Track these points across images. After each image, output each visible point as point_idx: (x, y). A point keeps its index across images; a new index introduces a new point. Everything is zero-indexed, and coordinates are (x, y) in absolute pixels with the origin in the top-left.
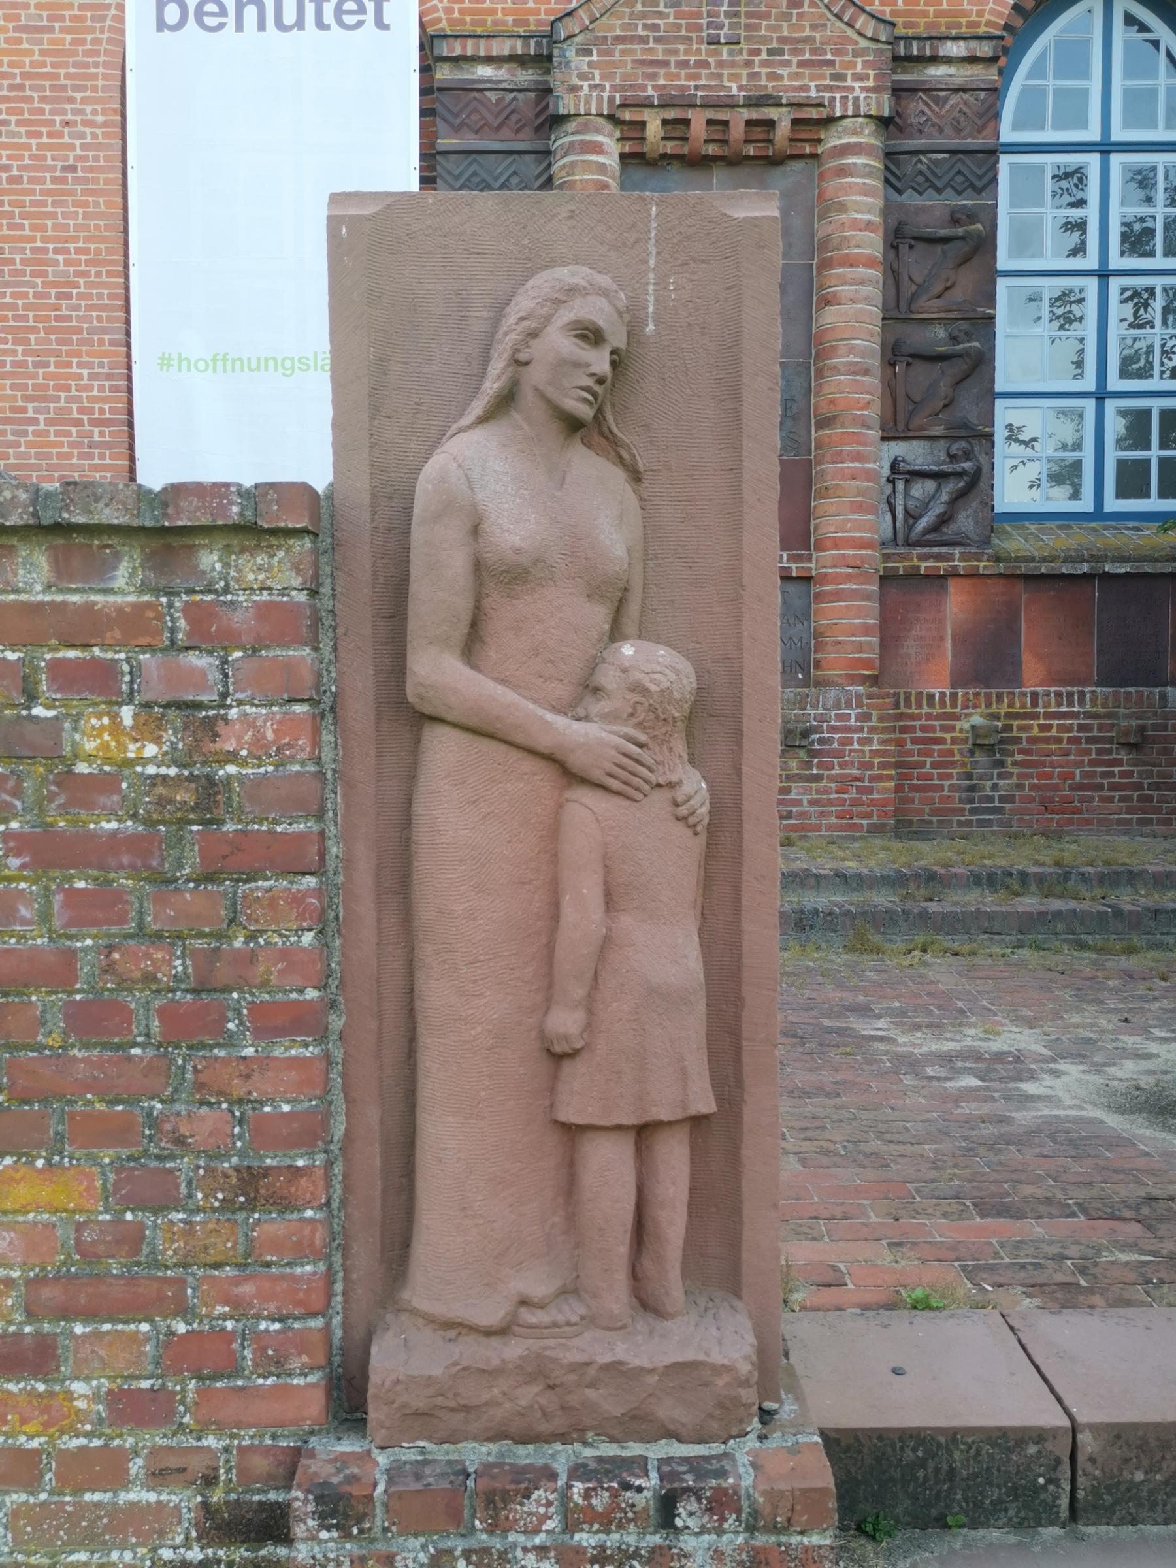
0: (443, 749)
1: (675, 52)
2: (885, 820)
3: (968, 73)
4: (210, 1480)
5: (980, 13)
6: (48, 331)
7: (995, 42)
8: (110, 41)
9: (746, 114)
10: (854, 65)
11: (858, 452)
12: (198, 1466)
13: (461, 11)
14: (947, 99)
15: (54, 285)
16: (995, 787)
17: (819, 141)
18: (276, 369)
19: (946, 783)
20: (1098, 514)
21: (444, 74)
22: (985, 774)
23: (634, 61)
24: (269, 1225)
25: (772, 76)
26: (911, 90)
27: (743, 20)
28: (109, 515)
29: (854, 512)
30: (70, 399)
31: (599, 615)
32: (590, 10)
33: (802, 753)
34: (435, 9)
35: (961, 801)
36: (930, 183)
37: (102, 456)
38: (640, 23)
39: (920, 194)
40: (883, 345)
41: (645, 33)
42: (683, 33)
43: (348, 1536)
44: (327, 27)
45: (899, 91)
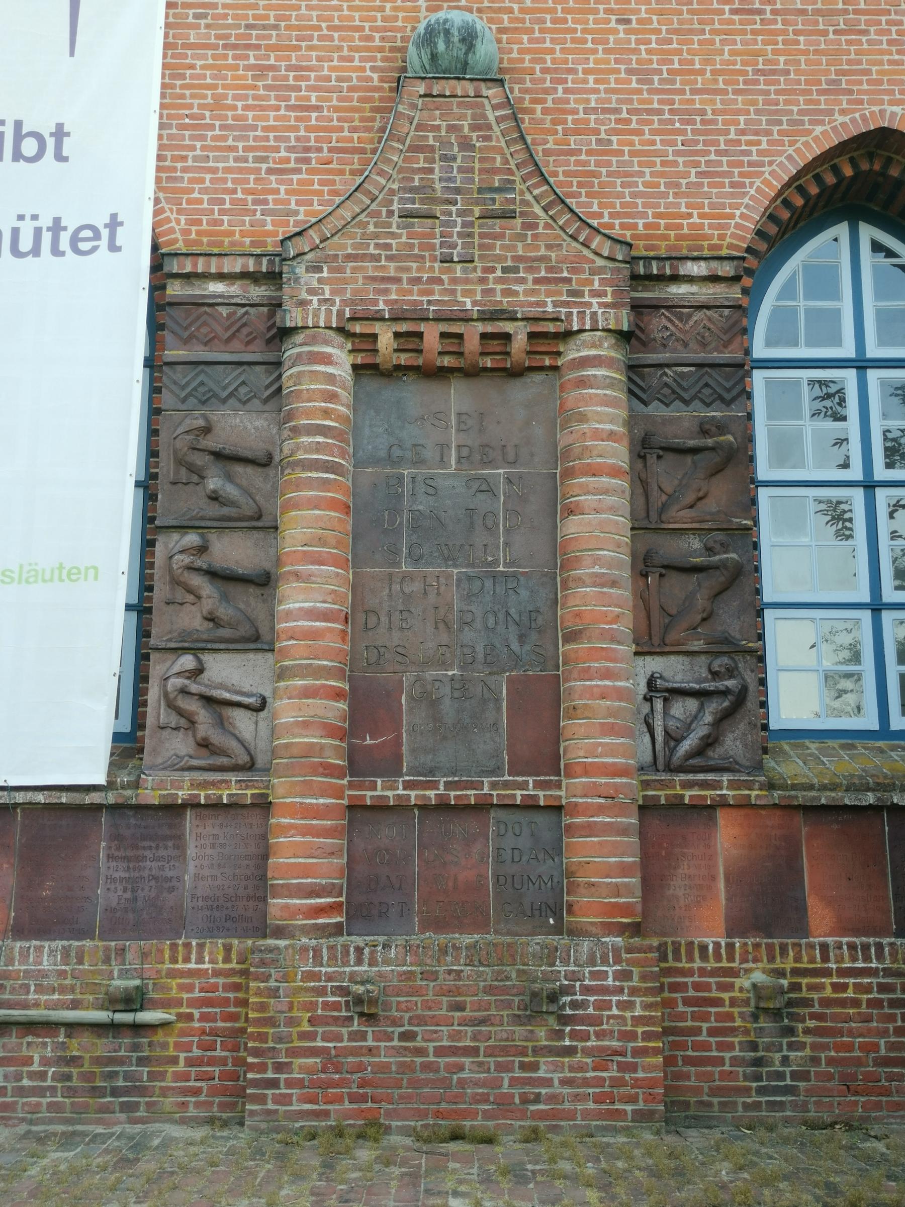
1: (408, 270)
2: (652, 1106)
3: (711, 291)
5: (722, 237)
7: (735, 262)
9: (481, 327)
10: (591, 282)
11: (608, 669)
13: (198, 233)
14: (690, 316)
16: (785, 1060)
17: (559, 354)
18: (44, 570)
19: (727, 1055)
20: (884, 731)
21: (175, 289)
22: (773, 1044)
23: (365, 278)
25: (507, 292)
26: (655, 307)
27: (476, 240)
29: (604, 734)
32: (320, 230)
33: (552, 1021)
34: (172, 231)
35: (746, 1078)
36: (675, 395)
38: (372, 242)
39: (667, 405)
40: (634, 555)
41: (377, 252)
42: (416, 251)
44: (63, 254)
45: (637, 308)
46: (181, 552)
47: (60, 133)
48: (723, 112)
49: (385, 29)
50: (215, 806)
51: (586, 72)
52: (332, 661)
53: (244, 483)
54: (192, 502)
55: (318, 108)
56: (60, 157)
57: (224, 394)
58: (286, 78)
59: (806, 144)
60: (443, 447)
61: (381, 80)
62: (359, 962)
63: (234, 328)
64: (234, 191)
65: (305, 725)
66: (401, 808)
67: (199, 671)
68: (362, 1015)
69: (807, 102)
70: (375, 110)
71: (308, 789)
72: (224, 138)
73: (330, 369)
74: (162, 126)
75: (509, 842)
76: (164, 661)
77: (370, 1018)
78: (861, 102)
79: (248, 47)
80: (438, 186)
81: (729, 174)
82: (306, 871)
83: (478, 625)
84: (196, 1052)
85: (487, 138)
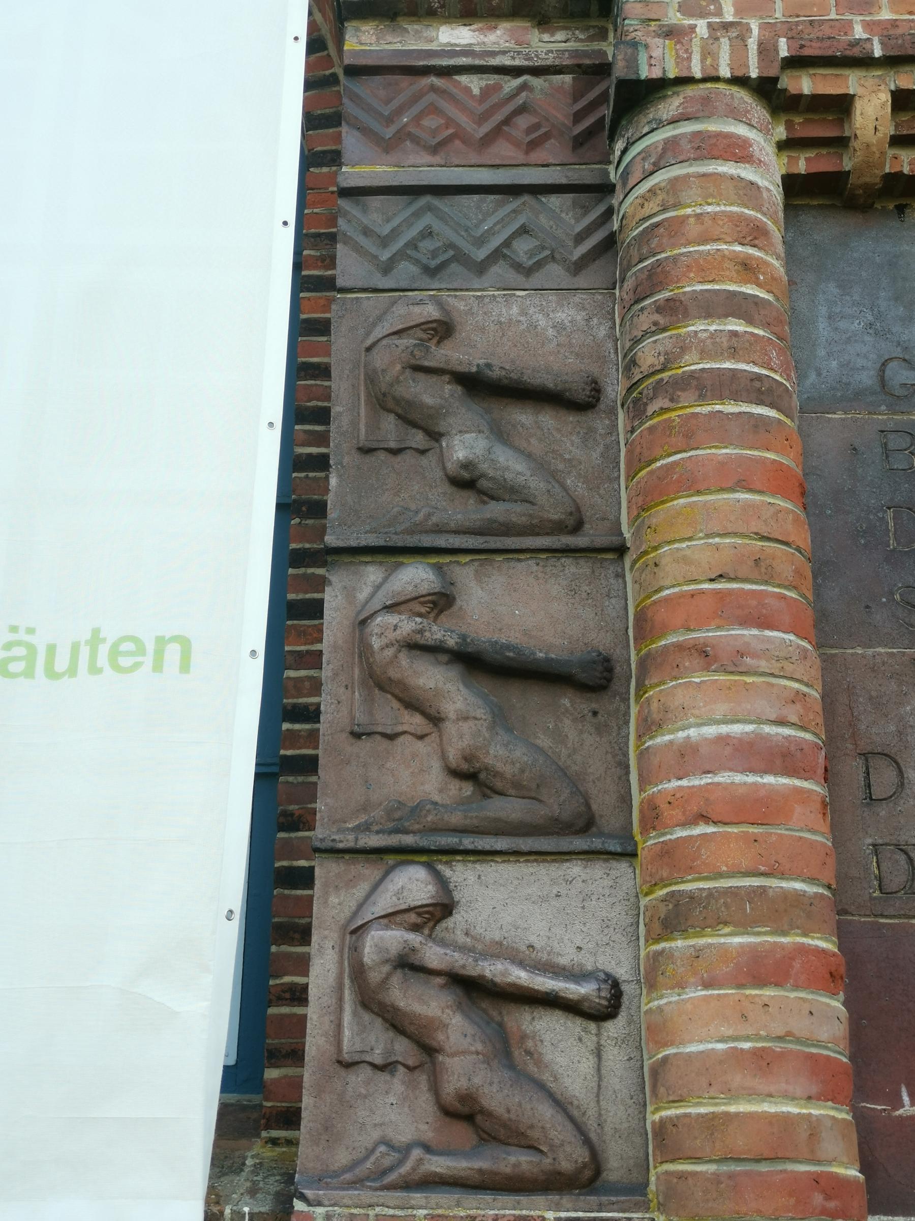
18: (51, 649)
44: (100, 671)
46: (389, 608)
52: (812, 880)
53: (536, 446)
54: (414, 495)
57: (481, 254)
63: (499, 117)
65: (763, 1061)
67: (442, 909)
73: (747, 173)
76: (351, 883)
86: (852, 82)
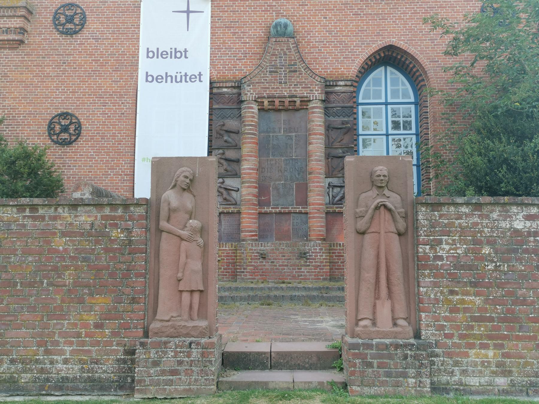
0: (164, 235)
1: (271, 85)
4: (125, 345)
5: (349, 74)
6: (115, 152)
8: (134, 84)
9: (289, 99)
12: (123, 343)
14: (340, 95)
15: (117, 141)
21: (215, 91)
24: (136, 306)
25: (295, 91)
26: (332, 93)
28: (118, 202)
29: (317, 196)
30: (119, 169)
31: (187, 216)
34: (214, 75)
36: (336, 115)
37: (126, 183)
40: (325, 154)
43: (144, 349)
45: (327, 93)
47: (186, 51)
48: (350, 41)
49: (265, 22)
50: (228, 213)
51: (316, 32)
54: (221, 143)
55: (249, 43)
56: (186, 57)
58: (241, 35)
59: (371, 49)
60: (280, 128)
61: (264, 35)
62: (262, 246)
64: (228, 65)
65: (249, 194)
66: (271, 213)
68: (262, 257)
69: (371, 38)
70: (263, 43)
71: (249, 209)
72: (226, 51)
73: (253, 110)
74: (211, 49)
75: (295, 221)
77: (264, 258)
78: (385, 38)
79: (231, 27)
80: (278, 64)
81: (351, 58)
82: (249, 227)
83: (288, 171)
84: (225, 267)
85: (290, 52)
86: (264, 100)
